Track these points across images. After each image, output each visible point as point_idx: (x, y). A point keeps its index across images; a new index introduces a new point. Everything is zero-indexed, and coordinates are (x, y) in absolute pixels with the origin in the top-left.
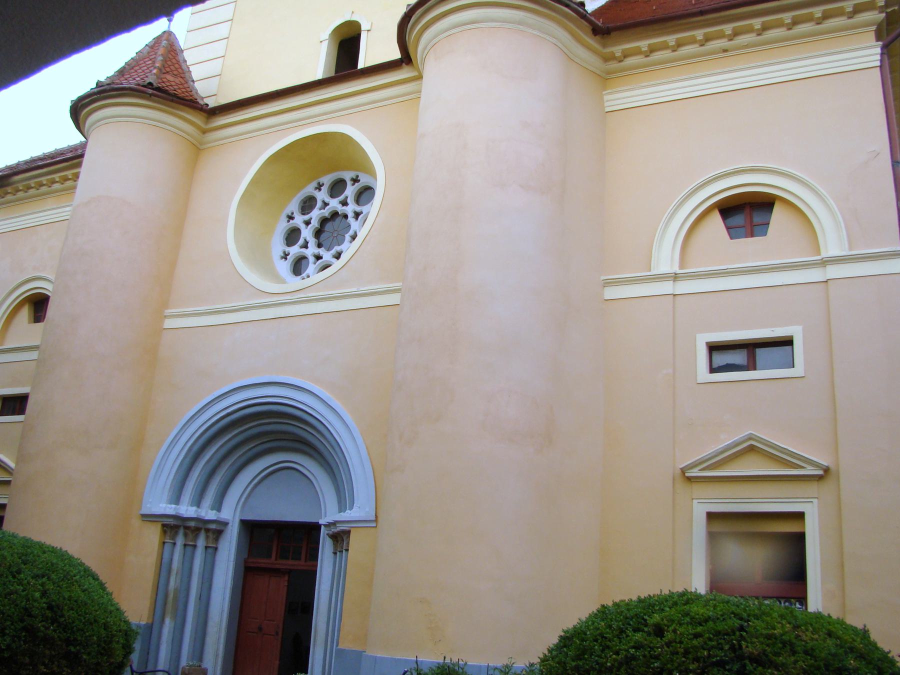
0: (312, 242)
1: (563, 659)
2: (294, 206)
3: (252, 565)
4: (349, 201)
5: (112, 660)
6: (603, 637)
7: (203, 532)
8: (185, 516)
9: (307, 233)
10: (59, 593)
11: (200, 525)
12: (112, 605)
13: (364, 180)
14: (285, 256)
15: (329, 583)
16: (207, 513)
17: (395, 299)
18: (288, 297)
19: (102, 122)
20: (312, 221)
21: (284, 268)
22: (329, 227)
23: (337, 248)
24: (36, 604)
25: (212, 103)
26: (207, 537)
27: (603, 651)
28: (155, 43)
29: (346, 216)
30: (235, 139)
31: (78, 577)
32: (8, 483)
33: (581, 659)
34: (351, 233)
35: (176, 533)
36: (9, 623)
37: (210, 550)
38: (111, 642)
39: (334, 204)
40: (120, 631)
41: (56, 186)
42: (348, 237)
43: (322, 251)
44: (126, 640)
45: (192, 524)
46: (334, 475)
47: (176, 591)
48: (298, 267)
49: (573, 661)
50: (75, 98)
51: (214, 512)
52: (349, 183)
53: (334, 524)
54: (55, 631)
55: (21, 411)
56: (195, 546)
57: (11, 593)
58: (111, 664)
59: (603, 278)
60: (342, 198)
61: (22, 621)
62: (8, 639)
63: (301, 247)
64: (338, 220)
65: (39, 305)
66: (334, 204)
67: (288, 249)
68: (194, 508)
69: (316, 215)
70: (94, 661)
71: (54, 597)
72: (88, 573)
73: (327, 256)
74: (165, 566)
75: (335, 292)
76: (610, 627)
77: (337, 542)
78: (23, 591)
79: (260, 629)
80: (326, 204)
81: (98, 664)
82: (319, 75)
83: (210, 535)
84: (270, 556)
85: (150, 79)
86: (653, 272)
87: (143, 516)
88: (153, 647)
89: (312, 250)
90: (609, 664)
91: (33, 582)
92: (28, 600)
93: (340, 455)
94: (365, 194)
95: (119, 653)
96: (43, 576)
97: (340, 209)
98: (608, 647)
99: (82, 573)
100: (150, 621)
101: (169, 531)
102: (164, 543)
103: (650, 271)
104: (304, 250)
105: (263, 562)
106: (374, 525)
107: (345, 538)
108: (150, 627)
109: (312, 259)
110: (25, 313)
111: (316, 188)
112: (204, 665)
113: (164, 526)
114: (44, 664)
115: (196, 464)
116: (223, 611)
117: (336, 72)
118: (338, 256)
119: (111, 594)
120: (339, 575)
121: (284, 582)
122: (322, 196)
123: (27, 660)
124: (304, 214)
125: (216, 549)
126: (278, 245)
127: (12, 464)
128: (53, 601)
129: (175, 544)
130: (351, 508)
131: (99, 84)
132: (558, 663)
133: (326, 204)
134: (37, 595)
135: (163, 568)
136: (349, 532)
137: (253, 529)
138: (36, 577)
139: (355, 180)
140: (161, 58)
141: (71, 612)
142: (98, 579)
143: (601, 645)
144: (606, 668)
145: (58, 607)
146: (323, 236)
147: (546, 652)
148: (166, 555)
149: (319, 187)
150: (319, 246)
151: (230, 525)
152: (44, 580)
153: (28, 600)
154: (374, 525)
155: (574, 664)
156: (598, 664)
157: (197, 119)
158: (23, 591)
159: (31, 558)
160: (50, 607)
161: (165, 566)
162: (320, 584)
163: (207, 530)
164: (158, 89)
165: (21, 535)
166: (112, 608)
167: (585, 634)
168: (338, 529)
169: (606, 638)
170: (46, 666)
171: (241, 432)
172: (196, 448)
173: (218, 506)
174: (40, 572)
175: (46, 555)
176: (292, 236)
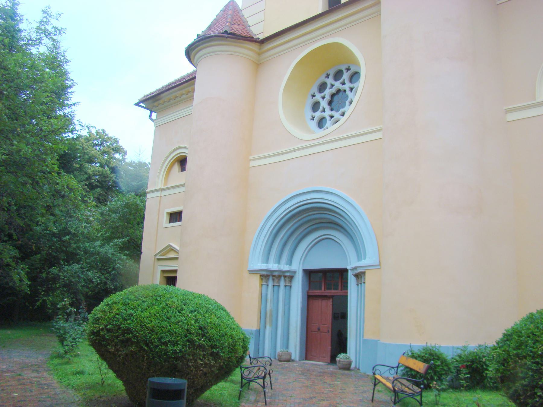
0: (327, 108)
1: (507, 349)
2: (315, 89)
4: (346, 82)
5: (237, 355)
6: (533, 334)
7: (283, 278)
8: (272, 269)
9: (324, 104)
10: (204, 320)
11: (281, 274)
12: (234, 325)
13: (353, 69)
14: (313, 118)
17: (379, 135)
18: (317, 141)
19: (203, 57)
20: (326, 96)
21: (313, 124)
22: (336, 98)
23: (342, 110)
24: (193, 327)
25: (261, 37)
26: (285, 280)
27: (534, 343)
28: (226, 8)
29: (345, 91)
30: (276, 56)
31: (214, 310)
32: (177, 258)
33: (519, 349)
34: (349, 100)
35: (268, 279)
36: (179, 338)
37: (287, 288)
38: (235, 345)
39: (338, 85)
40: (240, 339)
41: (184, 96)
42: (347, 103)
43: (333, 113)
44: (244, 343)
45: (276, 274)
46: (353, 240)
47: (271, 311)
48: (321, 123)
49: (514, 350)
50: (186, 46)
52: (345, 71)
53: (355, 268)
54: (204, 341)
55: (180, 220)
56: (279, 286)
57: (179, 322)
58: (237, 357)
59: (505, 108)
60: (341, 80)
61: (186, 336)
62: (180, 347)
63: (322, 112)
64: (341, 94)
65: (182, 162)
66: (338, 85)
67: (314, 114)
68: (277, 265)
69: (328, 92)
70: (227, 356)
71: (202, 322)
72: (220, 308)
73: (337, 115)
75: (344, 135)
76: (538, 328)
78: (185, 320)
79: (319, 329)
80: (333, 86)
81: (229, 358)
82: (320, 11)
83: (287, 279)
84: (321, 289)
85: (227, 29)
86: (538, 100)
87: (249, 271)
88: (261, 342)
89: (328, 113)
90: (540, 352)
91: (190, 315)
92: (188, 325)
93: (356, 228)
94: (355, 76)
95: (241, 351)
96: (195, 311)
97: (341, 87)
98: (537, 341)
99: (216, 308)
100: (258, 328)
101: (264, 278)
103: (535, 100)
104: (323, 113)
105: (317, 292)
106: (378, 267)
108: (258, 331)
109: (328, 118)
110: (177, 167)
111: (326, 77)
113: (261, 276)
114: (200, 359)
116: (297, 320)
117: (329, 7)
118: (343, 114)
119: (233, 318)
120: (361, 297)
121: (330, 302)
122: (330, 81)
123: (191, 357)
124: (320, 93)
125: (291, 286)
126: (309, 113)
127: (178, 248)
128: (202, 324)
130: (365, 258)
131: (198, 36)
132: (504, 351)
133: (333, 86)
134: (193, 322)
135: (263, 299)
137: (309, 274)
138: (191, 312)
139: (348, 69)
140: (230, 16)
141: (212, 330)
142: (225, 311)
143: (532, 339)
144: (538, 355)
145: (205, 327)
146: (333, 104)
147: (495, 344)
149: (328, 76)
150: (332, 110)
151: (297, 273)
152: (196, 313)
153: (188, 325)
155: (515, 352)
156: (531, 352)
157: (254, 47)
158: (185, 320)
159: (187, 301)
160: (201, 328)
164: (231, 34)
165: (182, 289)
166: (235, 327)
167: (521, 332)
169: (535, 335)
170: (201, 360)
172: (274, 231)
173: (290, 262)
174: (193, 309)
175: (196, 299)
176: (316, 106)
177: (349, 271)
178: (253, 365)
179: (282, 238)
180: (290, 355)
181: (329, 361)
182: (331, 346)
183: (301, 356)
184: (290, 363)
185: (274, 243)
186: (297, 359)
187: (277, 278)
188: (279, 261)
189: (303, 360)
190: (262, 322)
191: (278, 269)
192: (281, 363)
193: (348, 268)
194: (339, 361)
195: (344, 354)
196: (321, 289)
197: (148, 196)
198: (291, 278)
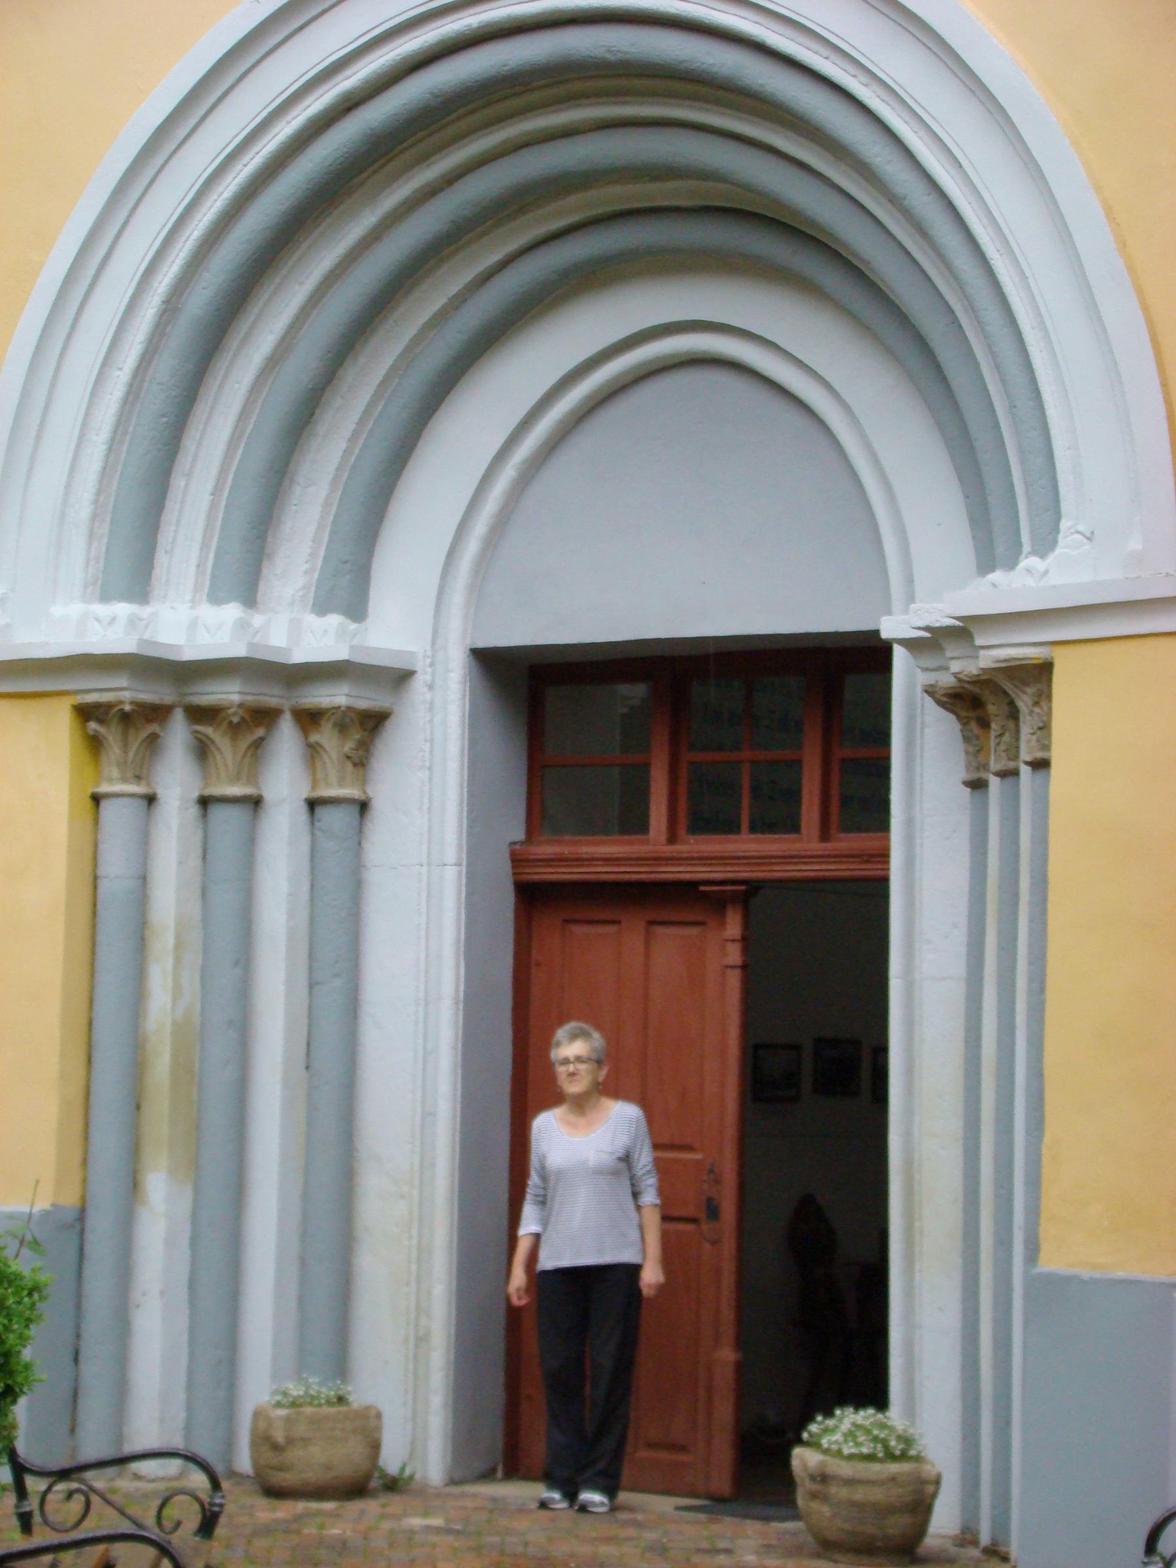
11: (271, 696)
15: (959, 938)
16: (295, 626)
26: (313, 752)
37: (334, 818)
45: (228, 693)
47: (189, 1038)
51: (334, 620)
53: (962, 632)
68: (232, 611)
77: (984, 724)
83: (326, 736)
84: (633, 821)
100: (70, 1199)
101: (111, 735)
102: (96, 799)
105: (604, 855)
107: (1024, 702)
112: (362, 1394)
113: (85, 713)
115: (178, 482)
120: (1011, 897)
121: (724, 945)
125: (363, 806)
129: (151, 800)
130: (1046, 543)
135: (107, 927)
136: (1044, 670)
137: (540, 693)
148: (116, 865)
151: (419, 684)
162: (909, 1112)
163: (309, 719)
168: (987, 659)
171: (431, 192)
173: (348, 585)
177: (899, 655)
178: (41, 1537)
179: (273, 362)
180: (368, 1428)
181: (722, 1482)
182: (740, 1343)
183: (463, 1440)
184: (371, 1506)
185: (201, 410)
186: (433, 1467)
187: (235, 730)
188: (243, 574)
189: (487, 1476)
190: (108, 1143)
191: (239, 650)
192: (285, 1510)
193: (890, 628)
194: (823, 1478)
195: (866, 1416)
196: (633, 821)
197: (739, 937)
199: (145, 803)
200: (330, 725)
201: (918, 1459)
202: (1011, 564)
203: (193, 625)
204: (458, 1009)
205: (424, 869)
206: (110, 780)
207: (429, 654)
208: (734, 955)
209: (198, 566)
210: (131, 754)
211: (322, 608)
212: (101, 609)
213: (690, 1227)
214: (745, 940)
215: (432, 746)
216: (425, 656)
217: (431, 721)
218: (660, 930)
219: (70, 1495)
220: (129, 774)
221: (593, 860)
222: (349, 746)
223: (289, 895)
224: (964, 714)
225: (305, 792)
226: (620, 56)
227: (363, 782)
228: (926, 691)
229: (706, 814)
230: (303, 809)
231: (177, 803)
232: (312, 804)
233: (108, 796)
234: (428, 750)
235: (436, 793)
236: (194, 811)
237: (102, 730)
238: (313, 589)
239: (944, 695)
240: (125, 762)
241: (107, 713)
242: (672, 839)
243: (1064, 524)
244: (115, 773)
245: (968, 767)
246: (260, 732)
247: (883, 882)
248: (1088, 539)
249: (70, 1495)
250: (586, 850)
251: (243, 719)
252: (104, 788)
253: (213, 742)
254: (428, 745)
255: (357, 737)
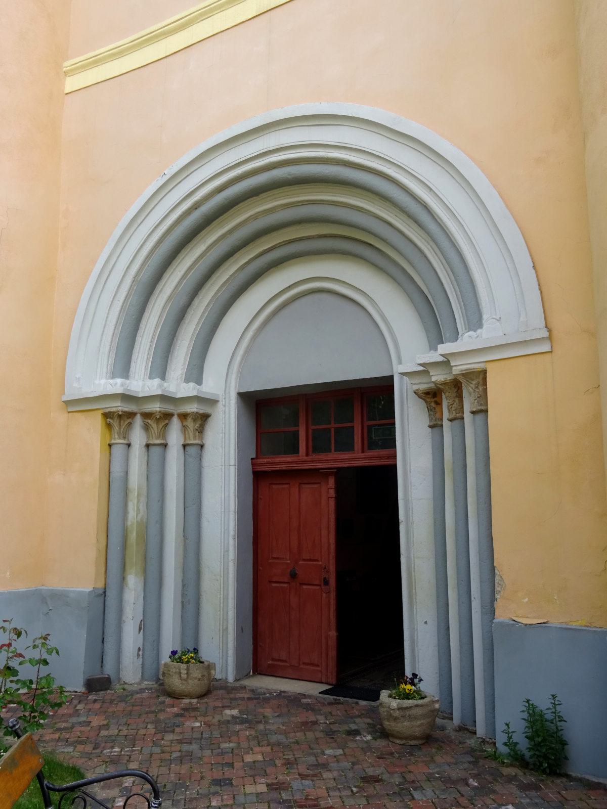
3: (267, 468)
7: (175, 421)
11: (169, 408)
26: (184, 428)
47: (144, 527)
51: (192, 385)
68: (157, 381)
74: (116, 485)
79: (294, 576)
83: (189, 423)
84: (350, 447)
87: (68, 403)
100: (101, 585)
101: (115, 423)
102: (110, 445)
105: (285, 461)
113: (107, 415)
125: (202, 446)
129: (129, 445)
135: (114, 488)
137: (260, 406)
148: (117, 469)
154: (546, 347)
161: (116, 485)
163: (183, 417)
173: (196, 373)
182: (338, 629)
183: (239, 666)
187: (158, 421)
190: (114, 565)
191: (159, 392)
198: (203, 419)
199: (127, 446)
200: (190, 419)
201: (143, 422)
202: (456, 337)
203: (143, 386)
204: (235, 515)
205: (223, 467)
206: (115, 439)
207: (224, 395)
208: (332, 493)
209: (146, 367)
210: (122, 430)
211: (187, 380)
212: (111, 381)
213: (318, 587)
214: (337, 490)
215: (225, 426)
216: (222, 396)
217: (225, 417)
218: (303, 486)
219: (95, 701)
220: (121, 437)
221: (280, 463)
222: (197, 425)
223: (177, 477)
224: (428, 400)
225: (182, 442)
226: (293, 176)
227: (201, 438)
228: (415, 393)
229: (318, 445)
230: (182, 448)
231: (138, 446)
232: (184, 446)
233: (114, 444)
234: (224, 426)
235: (225, 445)
236: (144, 449)
237: (111, 421)
238: (184, 375)
239: (422, 393)
240: (120, 433)
241: (113, 416)
242: (307, 455)
243: (485, 317)
244: (116, 437)
245: (431, 420)
246: (167, 421)
247: (395, 467)
248: (498, 320)
249: (95, 701)
250: (278, 460)
251: (160, 416)
252: (113, 441)
253: (151, 425)
254: (224, 425)
255: (200, 423)
